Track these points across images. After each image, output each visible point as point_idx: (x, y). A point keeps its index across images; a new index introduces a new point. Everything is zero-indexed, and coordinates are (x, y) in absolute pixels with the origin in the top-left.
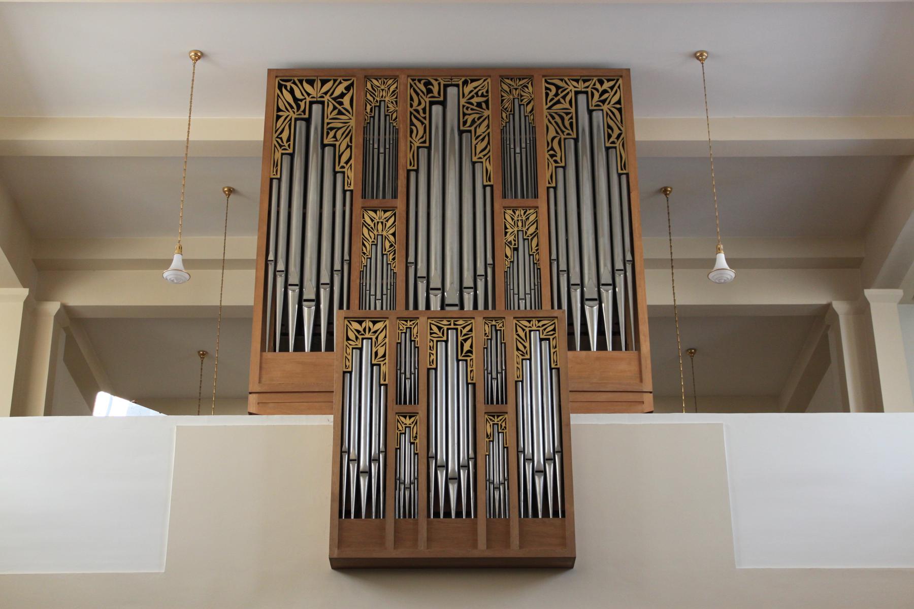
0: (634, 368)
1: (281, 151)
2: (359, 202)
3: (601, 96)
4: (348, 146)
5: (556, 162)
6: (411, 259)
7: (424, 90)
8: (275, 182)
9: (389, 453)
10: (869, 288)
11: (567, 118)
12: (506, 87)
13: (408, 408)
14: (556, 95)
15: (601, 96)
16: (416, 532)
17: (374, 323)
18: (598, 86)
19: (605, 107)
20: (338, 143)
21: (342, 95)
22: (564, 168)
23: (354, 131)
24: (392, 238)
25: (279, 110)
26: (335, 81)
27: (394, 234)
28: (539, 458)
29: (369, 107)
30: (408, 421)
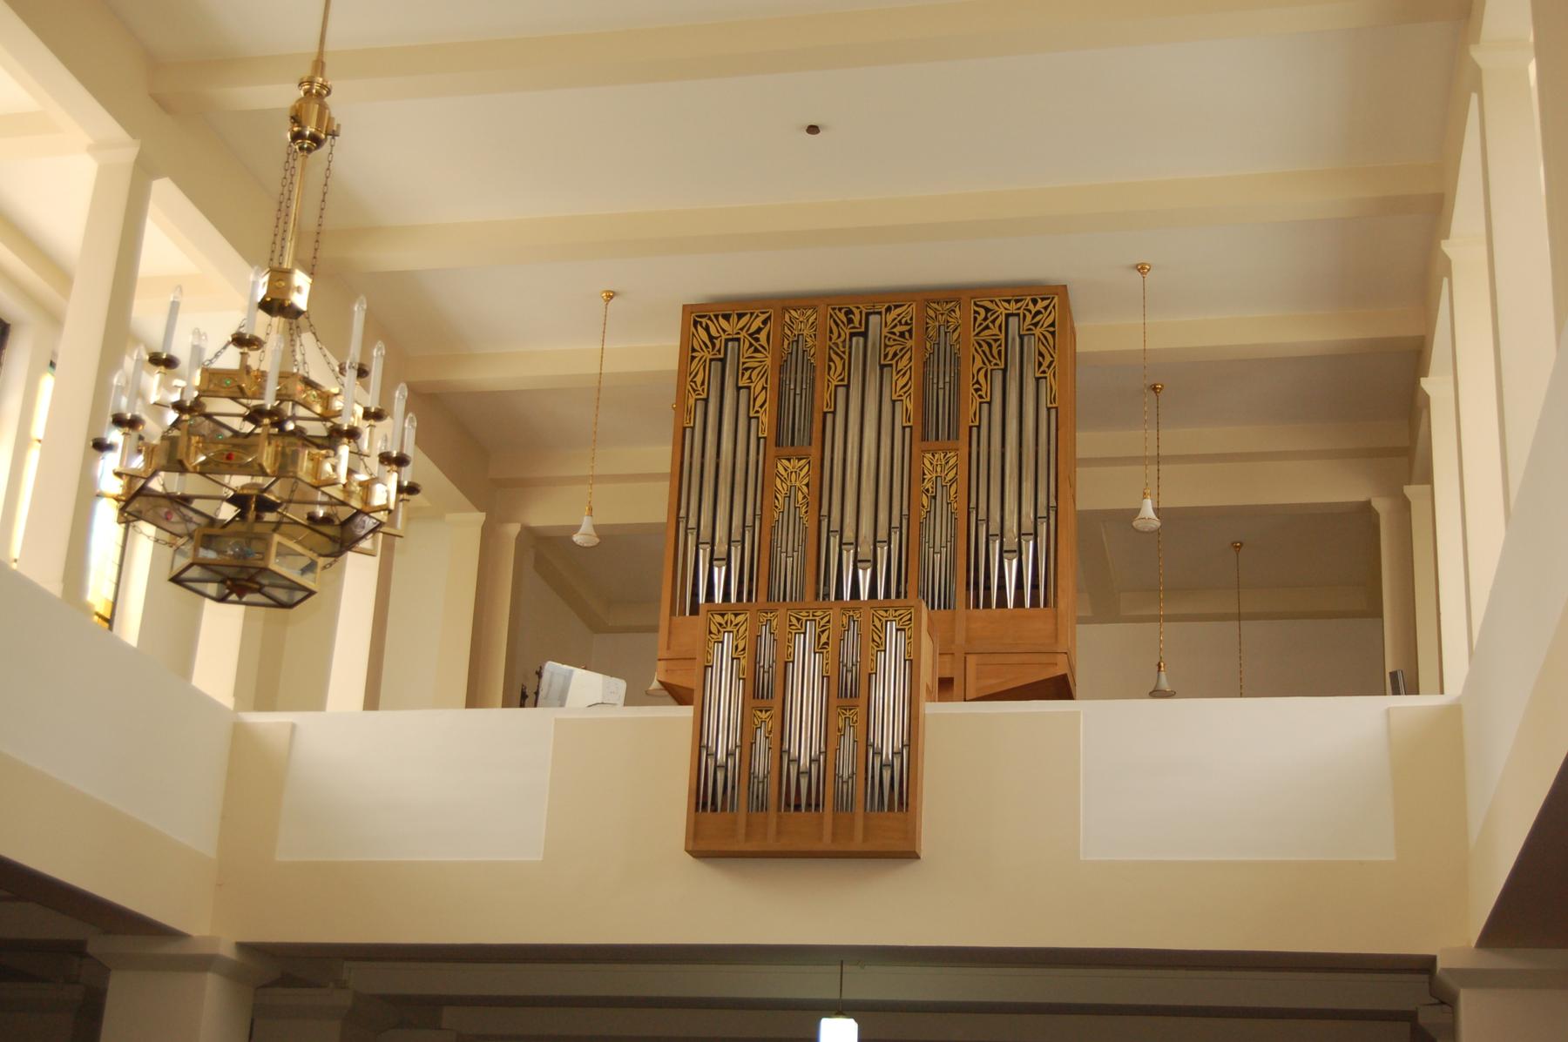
2: (772, 449)
6: (824, 511)
9: (747, 745)
11: (995, 346)
12: (931, 313)
14: (986, 319)
18: (1031, 306)
19: (1037, 331)
21: (759, 330)
22: (990, 403)
24: (805, 489)
25: (694, 350)
28: (887, 752)
30: (764, 715)
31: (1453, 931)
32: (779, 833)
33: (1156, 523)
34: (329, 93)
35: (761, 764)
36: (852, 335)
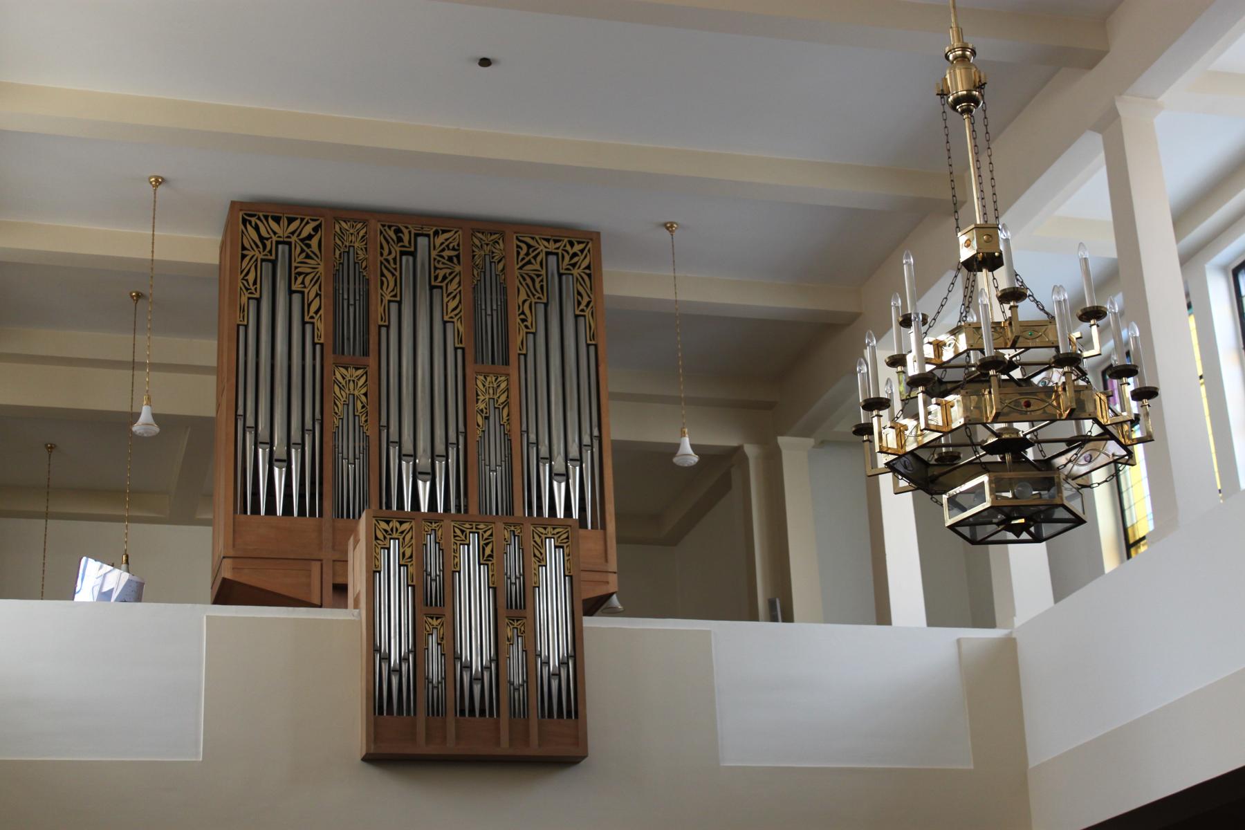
1: (248, 295)
2: (330, 358)
3: (571, 258)
4: (317, 295)
5: (527, 327)
7: (394, 237)
8: (242, 329)
9: (417, 650)
10: (782, 435)
11: (537, 280)
12: (477, 242)
14: (527, 254)
15: (571, 258)
17: (401, 523)
18: (568, 248)
19: (575, 272)
20: (306, 291)
21: (310, 237)
22: (534, 334)
23: (322, 278)
24: (363, 398)
25: (244, 248)
26: (302, 220)
27: (365, 394)
29: (337, 253)
30: (435, 622)
33: (695, 459)
34: (974, 53)
35: (434, 669)
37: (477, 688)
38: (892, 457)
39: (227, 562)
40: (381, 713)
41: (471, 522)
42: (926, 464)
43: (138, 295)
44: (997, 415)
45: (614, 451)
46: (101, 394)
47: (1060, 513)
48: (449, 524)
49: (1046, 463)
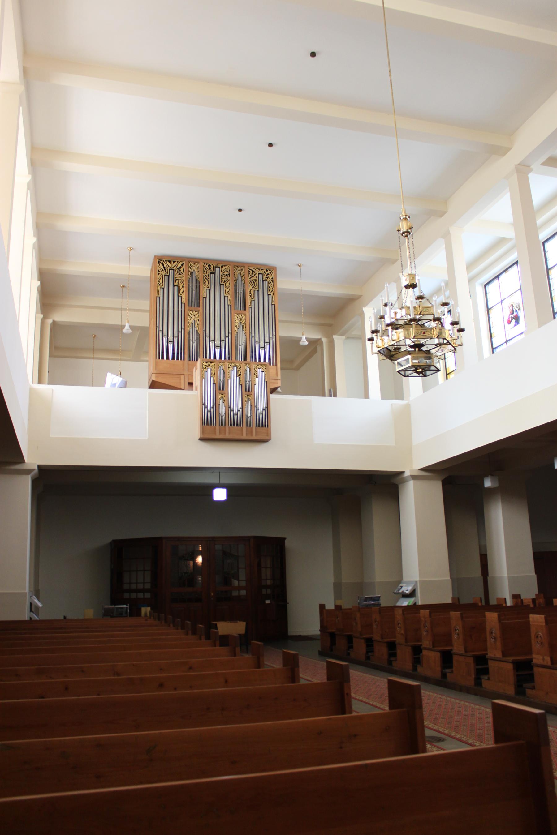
0: (275, 371)
9: (216, 404)
13: (222, 392)
16: (225, 430)
19: (268, 280)
21: (180, 267)
25: (159, 271)
30: (222, 396)
31: (33, 455)
32: (229, 433)
33: (307, 343)
35: (222, 410)
36: (211, 273)
37: (236, 417)
38: (380, 349)
39: (154, 375)
40: (205, 424)
41: (234, 363)
42: (390, 351)
43: (124, 286)
44: (414, 336)
45: (280, 339)
46: (112, 319)
47: (433, 368)
48: (227, 364)
49: (428, 352)
